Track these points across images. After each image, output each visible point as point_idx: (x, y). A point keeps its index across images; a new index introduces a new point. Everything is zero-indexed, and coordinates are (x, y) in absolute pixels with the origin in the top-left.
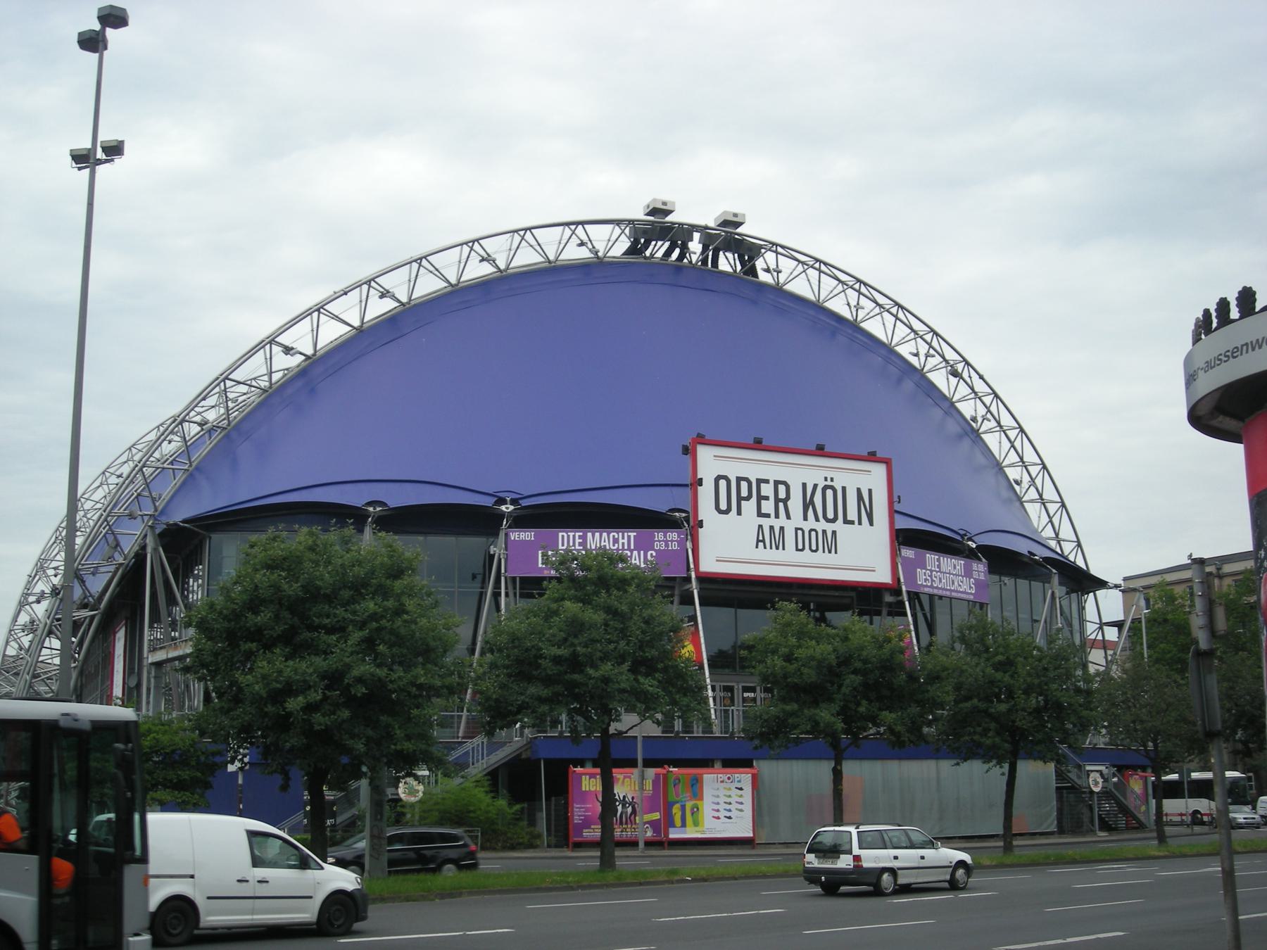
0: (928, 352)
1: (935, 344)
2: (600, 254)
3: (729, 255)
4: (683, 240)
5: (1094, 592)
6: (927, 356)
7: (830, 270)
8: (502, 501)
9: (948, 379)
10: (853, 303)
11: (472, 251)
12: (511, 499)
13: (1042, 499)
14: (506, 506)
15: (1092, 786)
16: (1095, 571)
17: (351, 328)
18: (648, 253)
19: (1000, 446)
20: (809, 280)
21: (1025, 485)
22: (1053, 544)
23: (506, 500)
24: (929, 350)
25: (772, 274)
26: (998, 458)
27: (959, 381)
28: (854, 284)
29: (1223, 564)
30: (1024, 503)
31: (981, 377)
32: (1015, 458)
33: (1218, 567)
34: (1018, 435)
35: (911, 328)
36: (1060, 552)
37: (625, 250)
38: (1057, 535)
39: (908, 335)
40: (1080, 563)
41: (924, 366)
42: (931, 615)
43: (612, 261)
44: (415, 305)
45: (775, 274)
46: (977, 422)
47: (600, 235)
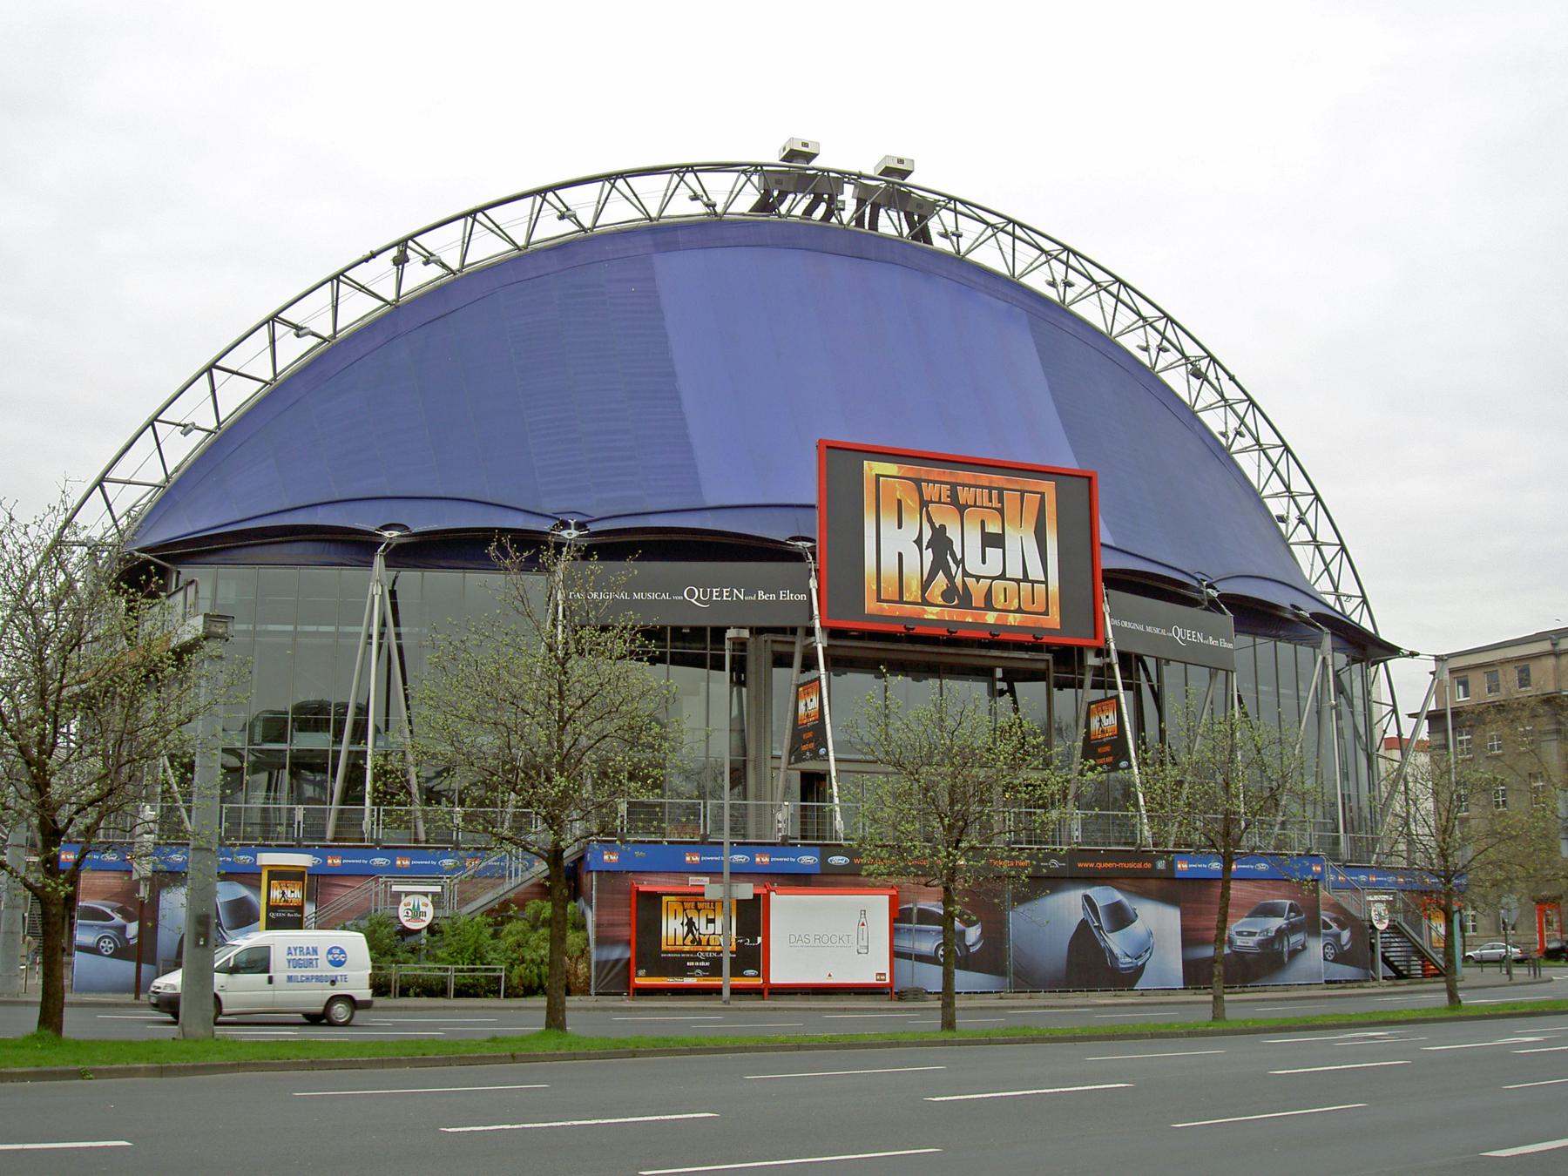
0: (1161, 344)
1: (1170, 333)
2: (719, 209)
3: (893, 214)
4: (830, 192)
5: (1384, 661)
6: (1161, 349)
7: (1027, 234)
8: (566, 525)
9: (1188, 381)
10: (1059, 278)
11: (545, 203)
12: (576, 523)
13: (1291, 492)
14: (569, 531)
15: (1375, 923)
16: (1383, 636)
17: (383, 303)
18: (783, 209)
19: (1259, 470)
20: (1000, 249)
21: (1293, 521)
22: (1331, 600)
23: (569, 524)
24: (1162, 341)
25: (951, 240)
26: (1257, 487)
27: (1202, 383)
28: (1060, 254)
29: (1559, 638)
30: (1291, 546)
31: (1232, 378)
32: (1247, 441)
33: (1555, 642)
34: (1311, 504)
35: (1139, 314)
36: (1341, 611)
37: (752, 205)
38: (1336, 589)
39: (1135, 323)
40: (1366, 624)
41: (1156, 363)
42: (1158, 686)
43: (735, 220)
44: (469, 274)
45: (954, 238)
46: (1228, 438)
47: (718, 186)
